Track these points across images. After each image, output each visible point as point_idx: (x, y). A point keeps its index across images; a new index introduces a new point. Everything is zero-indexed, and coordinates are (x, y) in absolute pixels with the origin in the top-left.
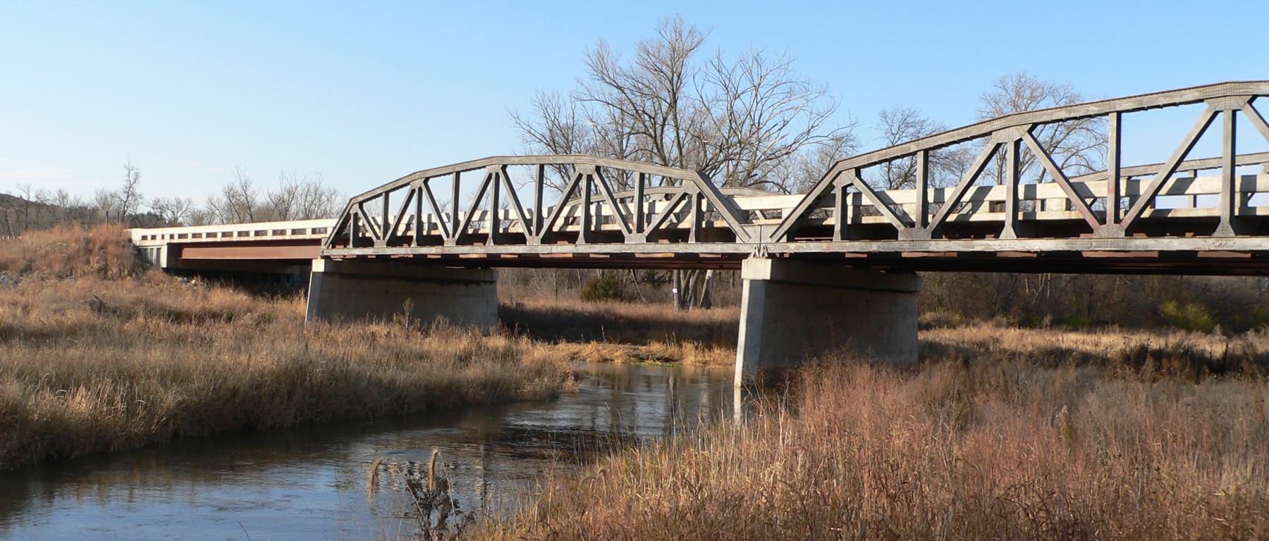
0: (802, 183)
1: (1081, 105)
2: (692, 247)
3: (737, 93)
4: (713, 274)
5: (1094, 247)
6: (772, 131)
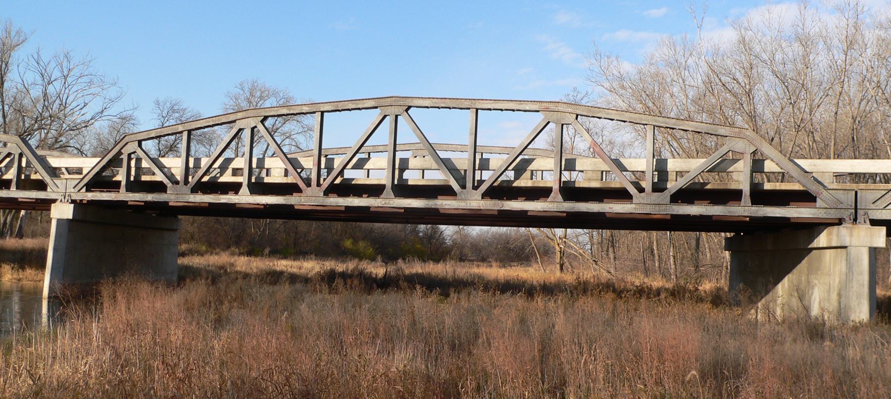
0: (96, 148)
2: (13, 193)
3: (50, 80)
4: (26, 213)
5: (303, 202)
6: (75, 110)
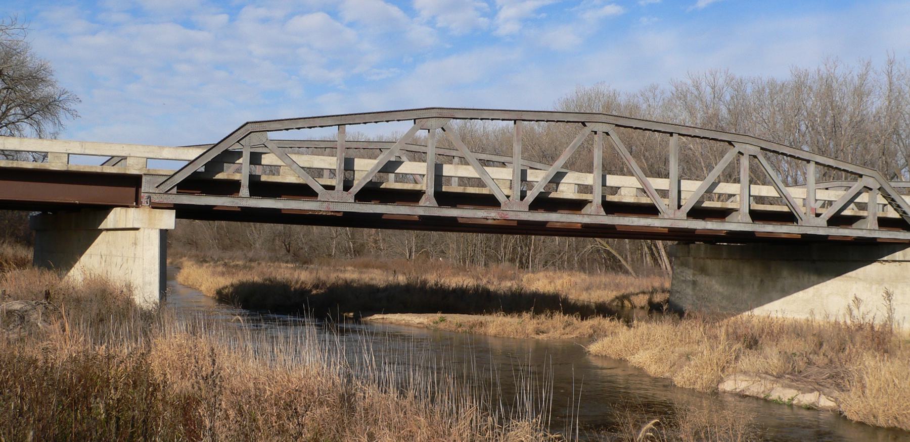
1: (610, 115)
